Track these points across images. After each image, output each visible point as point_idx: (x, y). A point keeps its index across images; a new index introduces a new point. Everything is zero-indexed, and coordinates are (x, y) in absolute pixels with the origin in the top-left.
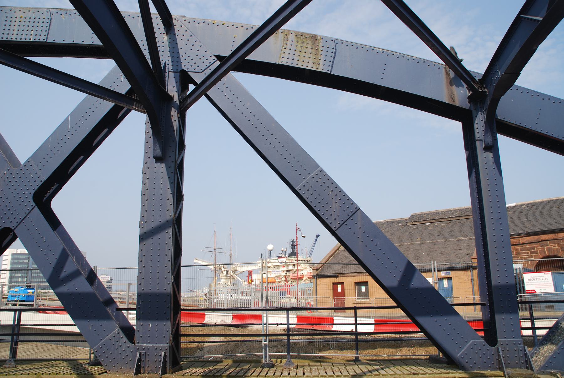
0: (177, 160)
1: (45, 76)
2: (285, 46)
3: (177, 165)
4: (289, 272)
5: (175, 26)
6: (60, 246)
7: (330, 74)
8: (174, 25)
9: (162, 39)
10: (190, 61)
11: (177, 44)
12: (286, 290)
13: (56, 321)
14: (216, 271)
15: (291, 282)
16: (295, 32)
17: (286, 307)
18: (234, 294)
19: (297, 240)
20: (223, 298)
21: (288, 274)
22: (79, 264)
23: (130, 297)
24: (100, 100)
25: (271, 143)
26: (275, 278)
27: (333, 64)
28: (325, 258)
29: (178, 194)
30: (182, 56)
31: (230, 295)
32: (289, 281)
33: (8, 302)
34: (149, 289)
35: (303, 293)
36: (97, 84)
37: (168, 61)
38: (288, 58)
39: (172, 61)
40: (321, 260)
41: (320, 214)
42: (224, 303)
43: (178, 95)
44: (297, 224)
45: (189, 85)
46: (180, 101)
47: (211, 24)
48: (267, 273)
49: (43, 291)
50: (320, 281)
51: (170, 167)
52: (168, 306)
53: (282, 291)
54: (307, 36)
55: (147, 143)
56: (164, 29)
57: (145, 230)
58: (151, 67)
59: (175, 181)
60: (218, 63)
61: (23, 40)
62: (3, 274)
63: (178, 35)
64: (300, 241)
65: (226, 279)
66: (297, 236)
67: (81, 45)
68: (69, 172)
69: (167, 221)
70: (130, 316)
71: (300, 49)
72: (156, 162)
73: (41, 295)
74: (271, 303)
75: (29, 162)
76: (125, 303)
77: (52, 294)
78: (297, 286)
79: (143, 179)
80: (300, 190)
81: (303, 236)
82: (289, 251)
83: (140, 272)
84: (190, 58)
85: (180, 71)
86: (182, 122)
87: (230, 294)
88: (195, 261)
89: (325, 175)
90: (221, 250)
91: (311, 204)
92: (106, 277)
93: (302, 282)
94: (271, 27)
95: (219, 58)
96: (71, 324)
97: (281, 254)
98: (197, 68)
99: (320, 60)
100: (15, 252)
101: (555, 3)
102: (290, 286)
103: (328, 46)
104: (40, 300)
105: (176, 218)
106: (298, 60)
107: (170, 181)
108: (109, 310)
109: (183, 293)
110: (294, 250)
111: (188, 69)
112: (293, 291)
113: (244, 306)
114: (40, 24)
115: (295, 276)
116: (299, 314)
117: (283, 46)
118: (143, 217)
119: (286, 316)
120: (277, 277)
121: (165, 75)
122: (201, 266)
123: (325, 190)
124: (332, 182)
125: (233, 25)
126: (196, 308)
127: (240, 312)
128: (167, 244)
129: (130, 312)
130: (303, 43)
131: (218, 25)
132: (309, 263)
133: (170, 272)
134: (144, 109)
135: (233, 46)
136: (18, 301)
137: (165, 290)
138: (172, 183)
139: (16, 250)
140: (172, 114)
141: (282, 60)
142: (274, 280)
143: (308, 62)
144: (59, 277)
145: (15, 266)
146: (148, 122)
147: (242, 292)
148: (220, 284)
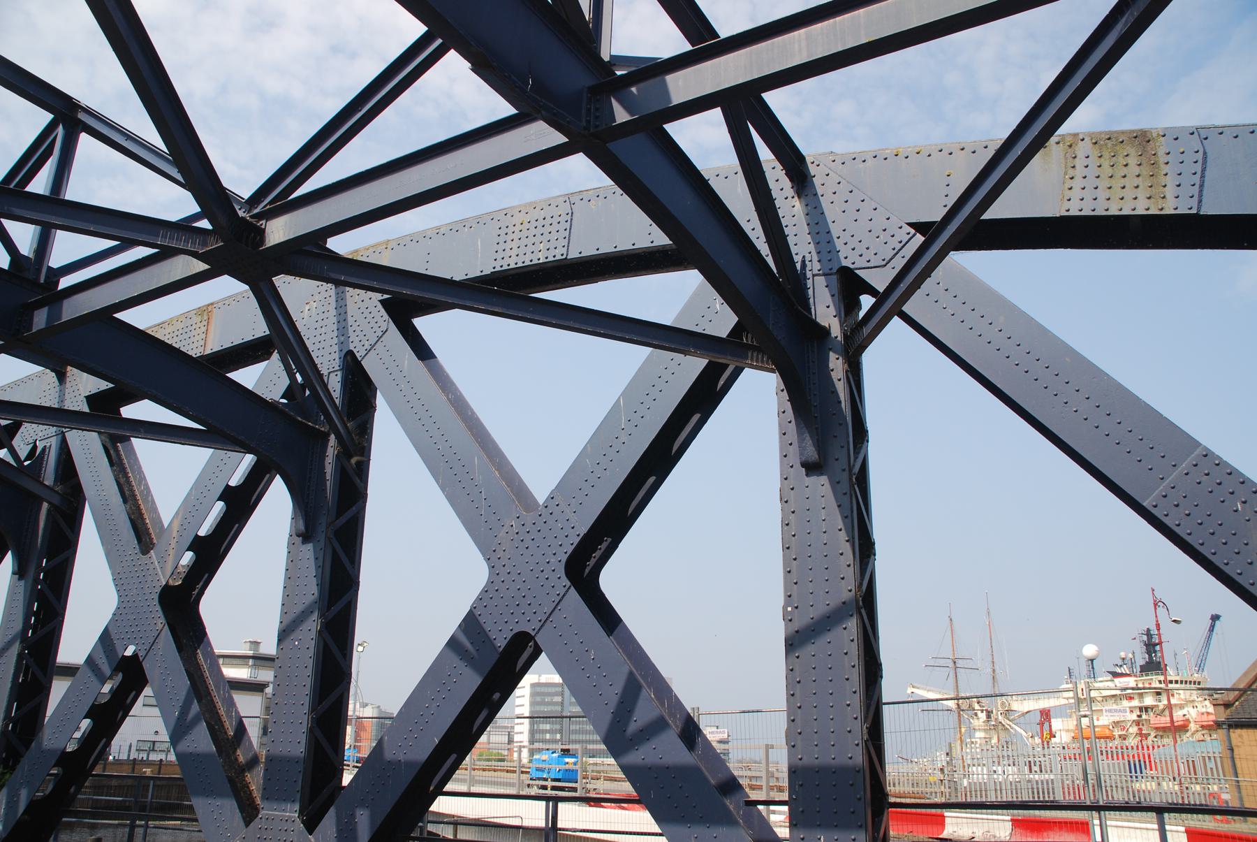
0: (854, 465)
1: (571, 324)
2: (1071, 172)
3: (854, 477)
4: (1146, 711)
6: (624, 668)
7: (1197, 216)
8: (813, 174)
9: (790, 208)
10: (856, 244)
11: (823, 213)
12: (1144, 758)
13: (645, 826)
14: (961, 713)
15: (1155, 737)
16: (1091, 135)
17: (1152, 804)
18: (1010, 768)
19: (1159, 630)
20: (985, 776)
21: (1144, 717)
22: (662, 704)
23: (770, 775)
24: (679, 357)
25: (1066, 403)
26: (1111, 727)
27: (1201, 191)
28: (1245, 674)
29: (861, 542)
30: (839, 238)
31: (1000, 769)
32: (1149, 734)
33: (531, 782)
34: (816, 757)
35: (1192, 766)
37: (810, 253)
38: (1082, 199)
39: (818, 253)
40: (1234, 681)
41: (1218, 563)
42: (986, 791)
43: (840, 321)
44: (1153, 590)
45: (860, 297)
46: (846, 337)
47: (891, 159)
48: (1092, 715)
49: (591, 760)
50: (1240, 736)
51: (838, 483)
52: (858, 796)
53: (1134, 761)
54: (1124, 138)
55: (784, 434)
56: (792, 188)
57: (796, 625)
58: (775, 271)
59: (852, 512)
60: (920, 239)
61: (513, 266)
62: (518, 724)
63: (822, 196)
64: (1168, 633)
66: (1157, 621)
67: (631, 252)
68: (630, 512)
69: (844, 603)
70: (773, 818)
71: (1110, 171)
72: (807, 475)
73: (590, 768)
74: (1107, 791)
75: (552, 498)
76: (760, 788)
77: (612, 768)
78: (1173, 748)
79: (782, 514)
80: (1155, 506)
81: (1173, 619)
82: (1141, 659)
83: (792, 718)
84: (857, 238)
85: (838, 271)
86: (854, 381)
87: (1000, 768)
88: (910, 690)
89: (1218, 465)
90: (969, 664)
91: (1188, 539)
92: (717, 732)
93: (1184, 737)
94: (1034, 136)
95: (919, 227)
96: (653, 831)
97: (1121, 666)
98: (873, 258)
99: (1165, 186)
100: (536, 681)
102: (1153, 747)
103: (1182, 150)
104: (588, 778)
105: (862, 594)
106: (1109, 199)
107: (841, 513)
108: (730, 803)
109: (891, 766)
110: (1153, 655)
111: (853, 263)
112: (1163, 760)
113: (1039, 797)
114: (555, 227)
115: (1164, 720)
116: (1191, 822)
117: (1066, 174)
118: (790, 596)
119: (1156, 826)
120: (1116, 724)
121: (806, 284)
122: (923, 701)
123: (1223, 502)
125: (941, 151)
126: (922, 801)
127: (1031, 812)
128: (846, 654)
129: (772, 808)
130: (1114, 156)
131: (907, 157)
132: (1200, 689)
133: (859, 718)
134: (770, 363)
135: (947, 196)
136: (549, 780)
137: (851, 758)
138: (846, 517)
139: (537, 676)
140: (831, 366)
141: (1067, 205)
142: (1107, 733)
143: (1136, 198)
144: (625, 731)
145: (538, 708)
146: (782, 390)
147: (1030, 762)
148: (973, 742)
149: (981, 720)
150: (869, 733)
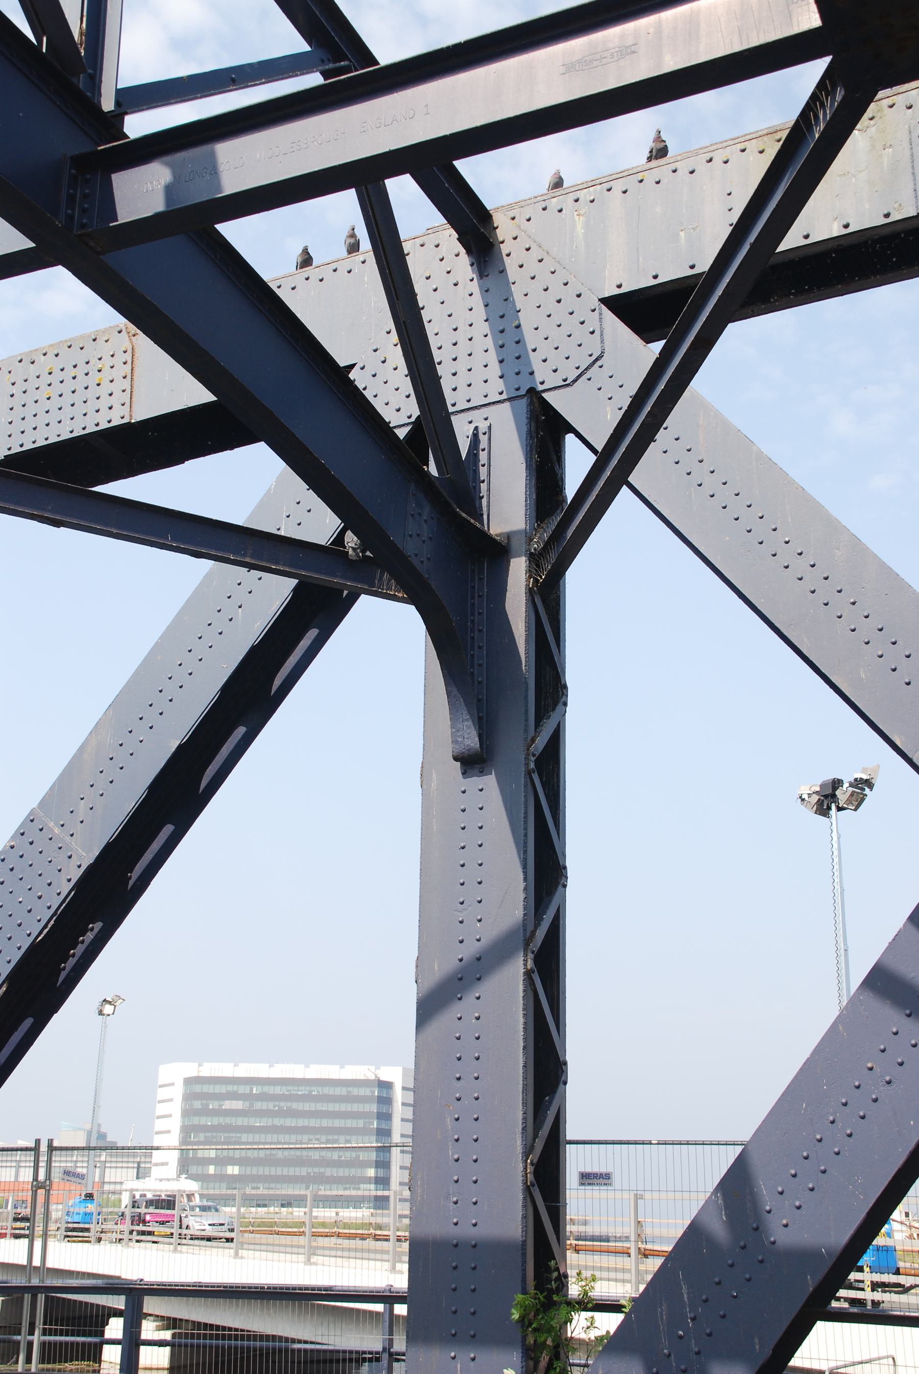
3: (533, 759)
5: (502, 242)
8: (501, 239)
101: (464, 515)
150: (536, 1173)
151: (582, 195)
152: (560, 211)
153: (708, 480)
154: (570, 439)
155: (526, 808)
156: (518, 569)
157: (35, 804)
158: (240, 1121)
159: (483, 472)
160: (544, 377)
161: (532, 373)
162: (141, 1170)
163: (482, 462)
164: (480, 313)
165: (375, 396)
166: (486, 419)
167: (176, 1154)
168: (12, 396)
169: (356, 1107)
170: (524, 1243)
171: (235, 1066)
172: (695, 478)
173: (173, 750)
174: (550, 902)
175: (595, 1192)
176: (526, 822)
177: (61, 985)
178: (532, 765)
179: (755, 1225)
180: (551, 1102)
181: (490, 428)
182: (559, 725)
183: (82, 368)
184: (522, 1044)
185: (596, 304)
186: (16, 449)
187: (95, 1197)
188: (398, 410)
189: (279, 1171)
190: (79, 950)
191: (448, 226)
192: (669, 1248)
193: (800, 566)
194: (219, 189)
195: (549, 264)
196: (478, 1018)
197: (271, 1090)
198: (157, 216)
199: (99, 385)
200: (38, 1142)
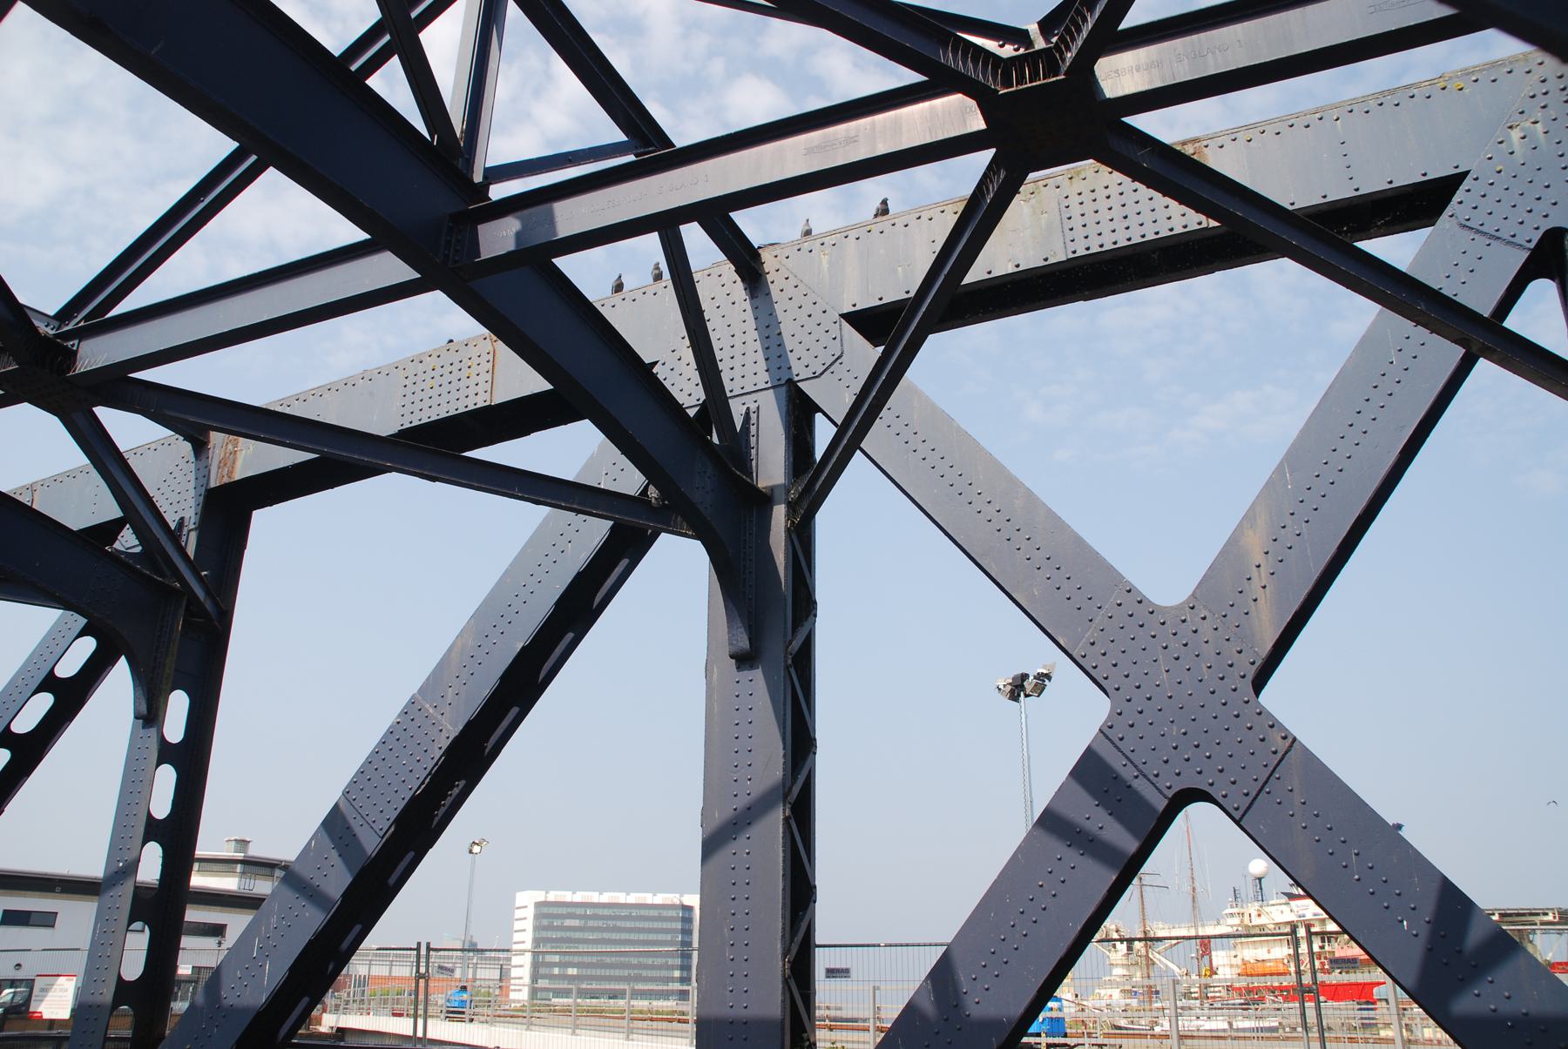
3: (790, 657)
5: (768, 273)
8: (767, 271)
26: (1286, 961)
36: (571, 479)
65: (1127, 966)
100: (542, 899)
101: (738, 473)
124: (1258, 711)
142: (1281, 968)
149: (1120, 954)
150: (792, 969)
151: (826, 240)
152: (811, 251)
153: (921, 447)
154: (819, 416)
155: (785, 694)
156: (779, 513)
157: (415, 691)
158: (578, 935)
159: (753, 440)
160: (799, 370)
161: (790, 368)
162: (503, 971)
163: (752, 434)
164: (751, 323)
165: (673, 385)
166: (755, 402)
167: (528, 956)
168: (405, 386)
169: (665, 925)
170: (783, 1021)
171: (573, 893)
172: (911, 446)
173: (519, 650)
174: (804, 764)
175: (837, 983)
176: (785, 705)
177: (436, 826)
178: (790, 662)
179: (955, 1003)
180: (804, 915)
181: (758, 408)
182: (810, 630)
183: (457, 366)
184: (781, 873)
185: (838, 317)
186: (407, 425)
187: (468, 988)
188: (690, 395)
189: (608, 972)
190: (448, 801)
191: (728, 262)
192: (889, 1026)
193: (990, 511)
194: (555, 233)
195: (802, 289)
196: (748, 853)
197: (601, 912)
198: (509, 254)
199: (468, 377)
200: (419, 944)
